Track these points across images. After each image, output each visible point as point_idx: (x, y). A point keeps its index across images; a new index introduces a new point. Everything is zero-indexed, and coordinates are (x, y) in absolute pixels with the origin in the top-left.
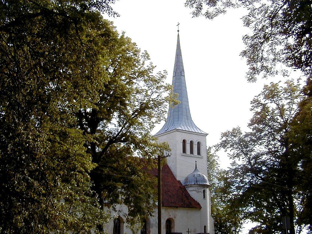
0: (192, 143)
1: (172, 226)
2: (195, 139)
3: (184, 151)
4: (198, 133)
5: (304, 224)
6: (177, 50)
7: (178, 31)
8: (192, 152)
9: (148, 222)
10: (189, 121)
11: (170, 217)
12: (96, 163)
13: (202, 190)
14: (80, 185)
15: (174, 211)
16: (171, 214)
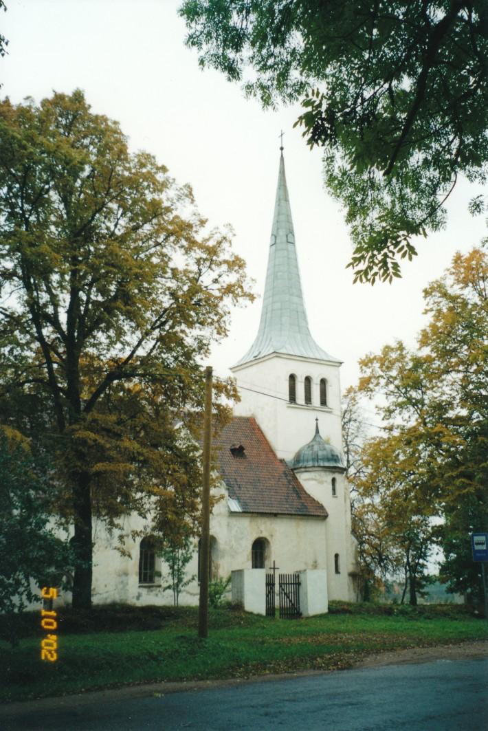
0: (308, 380)
1: (266, 554)
2: (317, 373)
7: (282, 149)
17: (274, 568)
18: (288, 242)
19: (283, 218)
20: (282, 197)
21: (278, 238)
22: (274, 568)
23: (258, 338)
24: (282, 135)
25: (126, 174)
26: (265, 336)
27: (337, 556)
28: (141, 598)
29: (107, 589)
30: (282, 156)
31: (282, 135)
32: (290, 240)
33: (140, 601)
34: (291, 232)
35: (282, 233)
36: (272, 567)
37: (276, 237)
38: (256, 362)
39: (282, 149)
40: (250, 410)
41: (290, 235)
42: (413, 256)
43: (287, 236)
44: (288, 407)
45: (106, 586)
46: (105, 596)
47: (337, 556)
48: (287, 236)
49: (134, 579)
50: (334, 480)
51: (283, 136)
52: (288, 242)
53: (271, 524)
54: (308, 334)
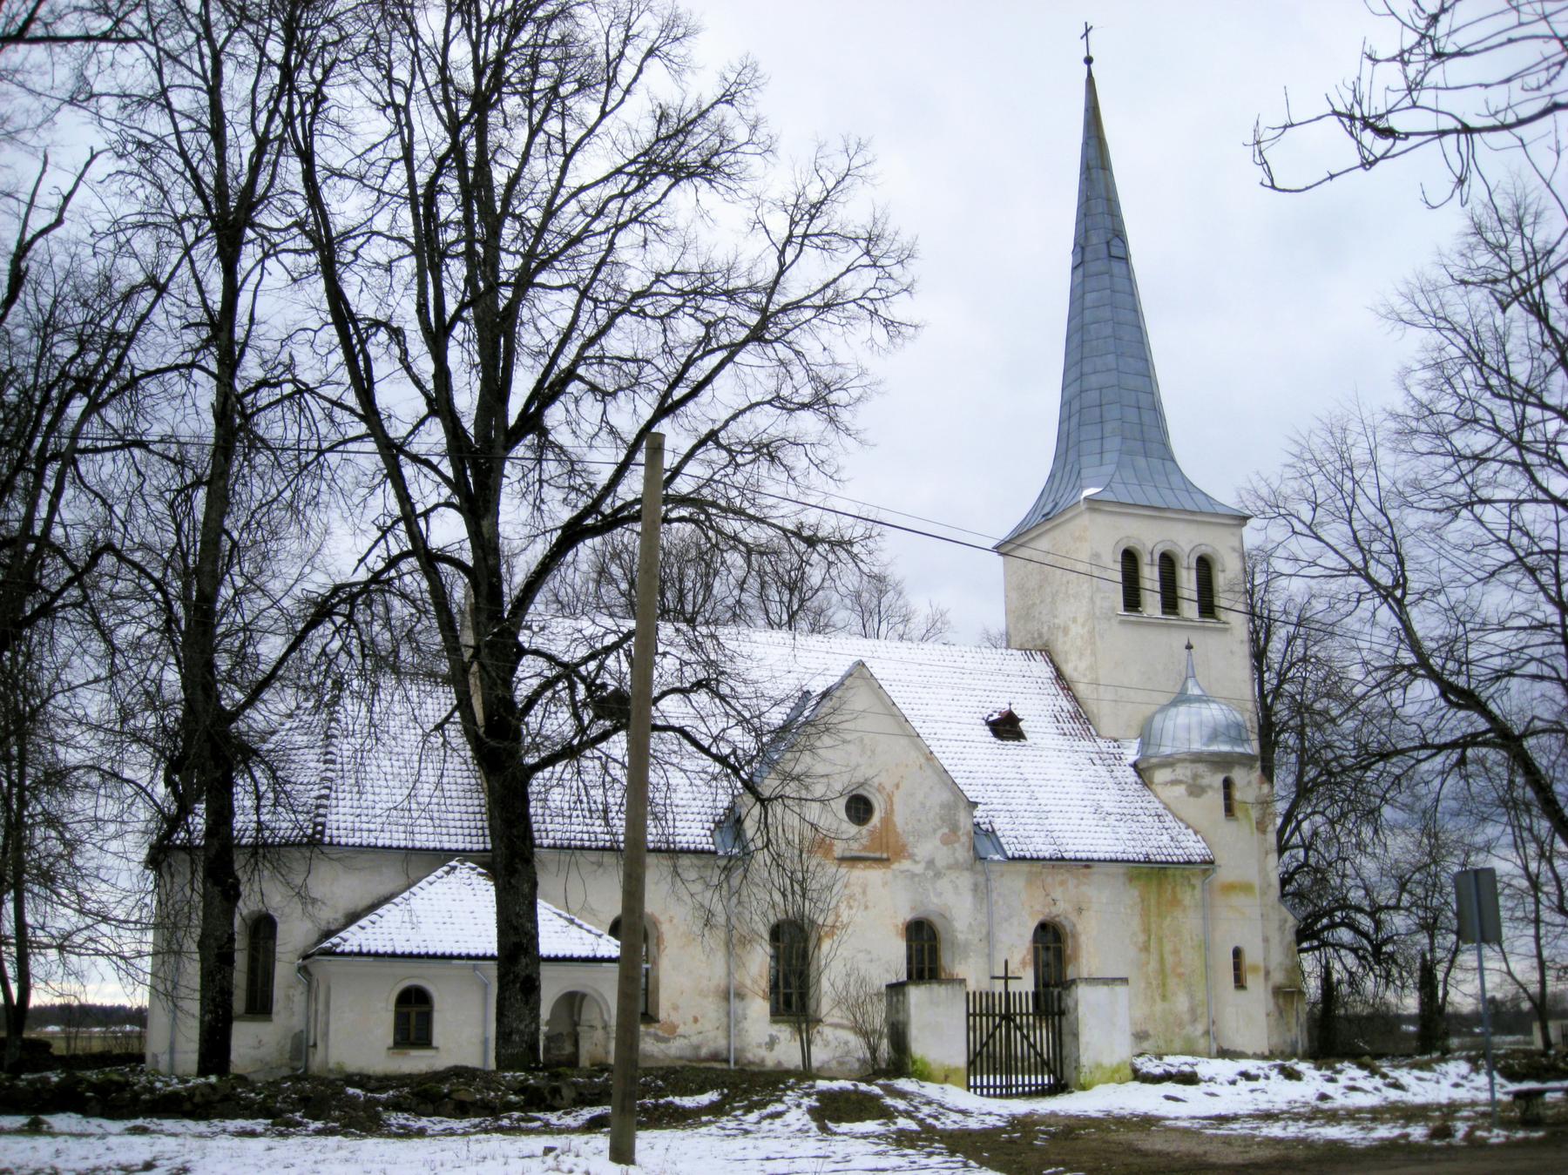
0: (1168, 563)
1: (1069, 952)
2: (1186, 541)
3: (1132, 600)
5: (489, 846)
6: (1086, 144)
7: (1089, 61)
8: (1170, 603)
9: (289, 1042)
10: (1175, 479)
11: (1055, 910)
12: (651, 675)
15: (1071, 883)
16: (1057, 893)
17: (1006, 978)
19: (1098, 206)
20: (1092, 163)
21: (1088, 250)
23: (1052, 476)
24: (1087, 31)
25: (226, 592)
26: (1068, 468)
27: (1237, 953)
28: (777, 1047)
30: (1090, 81)
31: (1087, 31)
32: (1114, 252)
33: (775, 1053)
34: (1119, 234)
37: (1083, 249)
39: (1089, 61)
40: (1041, 636)
41: (1116, 241)
42: (1436, 258)
44: (1122, 622)
45: (696, 1020)
46: (695, 1040)
47: (1237, 953)
49: (759, 1008)
50: (1228, 784)
51: (1090, 34)
53: (1077, 886)
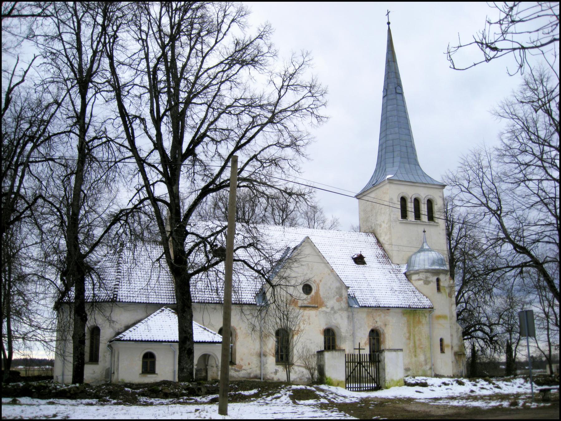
0: (417, 202)
1: (382, 340)
2: (423, 194)
3: (404, 215)
4: (429, 184)
6: (388, 53)
7: (389, 23)
8: (418, 216)
11: (377, 325)
13: (435, 279)
14: (86, 309)
15: (383, 315)
17: (359, 349)
18: (396, 93)
20: (390, 60)
21: (388, 90)
22: (359, 349)
23: (376, 171)
24: (388, 13)
26: (381, 168)
27: (441, 340)
28: (278, 374)
29: (250, 366)
31: (388, 13)
32: (398, 91)
35: (391, 87)
36: (358, 347)
37: (387, 90)
38: (374, 188)
40: (372, 228)
41: (398, 88)
43: (395, 88)
45: (249, 364)
46: (249, 371)
47: (441, 340)
48: (395, 88)
49: (271, 360)
50: (438, 280)
52: (396, 93)
53: (385, 316)
54: (417, 164)
